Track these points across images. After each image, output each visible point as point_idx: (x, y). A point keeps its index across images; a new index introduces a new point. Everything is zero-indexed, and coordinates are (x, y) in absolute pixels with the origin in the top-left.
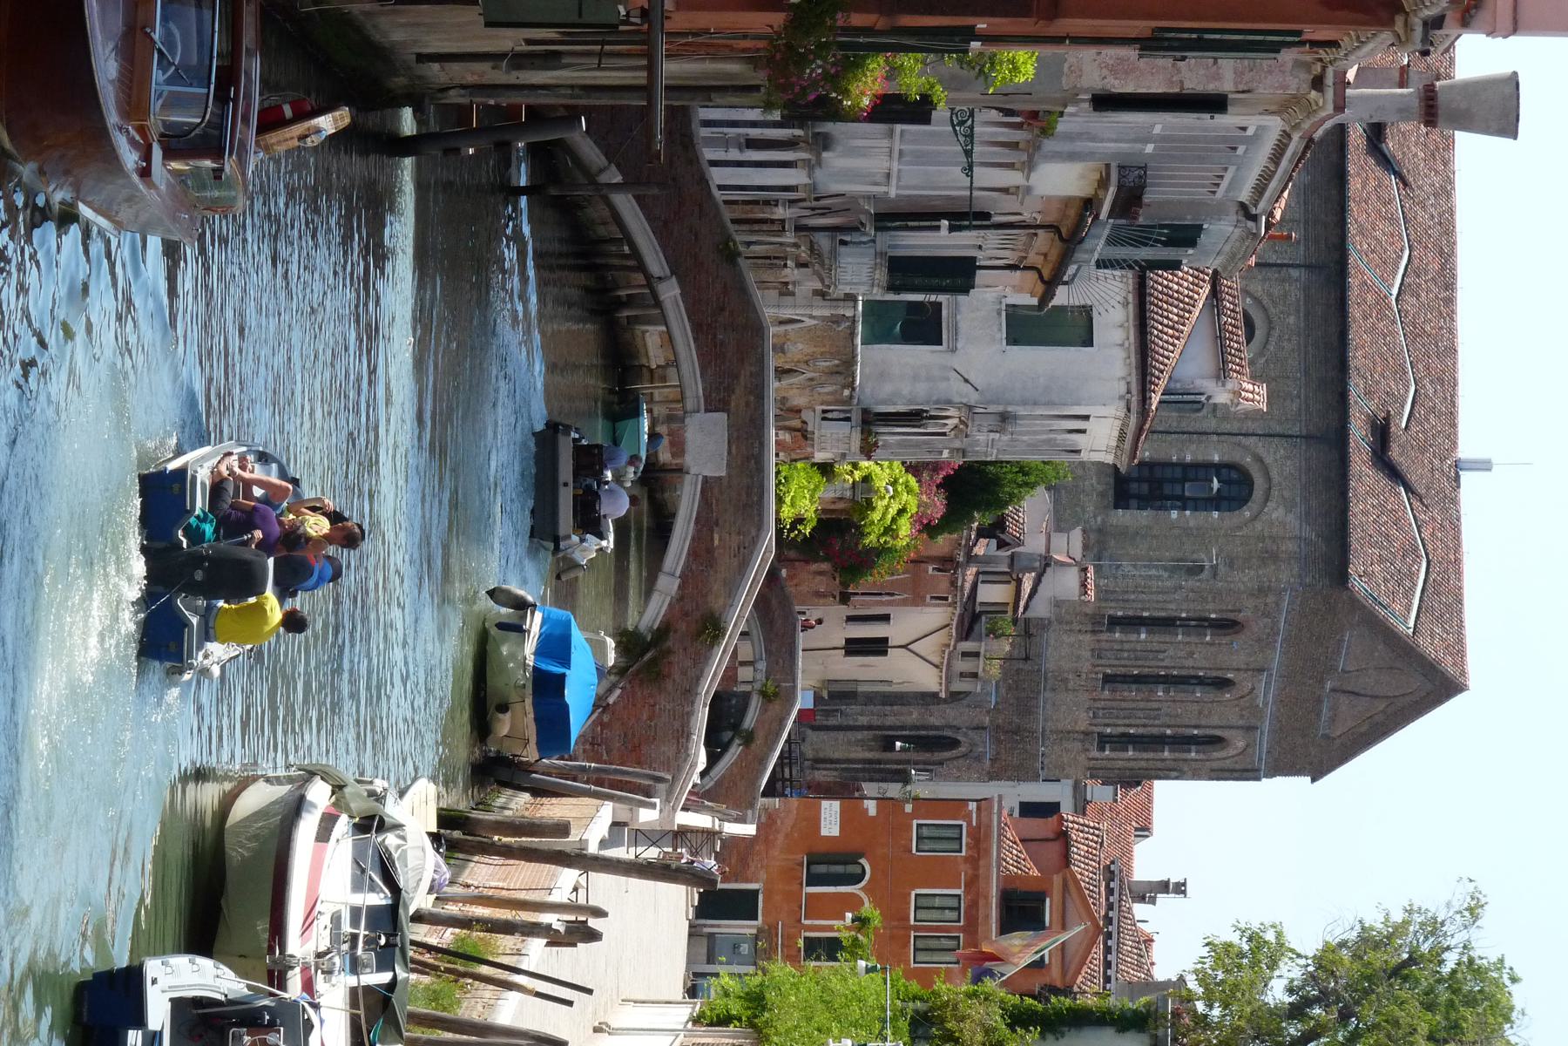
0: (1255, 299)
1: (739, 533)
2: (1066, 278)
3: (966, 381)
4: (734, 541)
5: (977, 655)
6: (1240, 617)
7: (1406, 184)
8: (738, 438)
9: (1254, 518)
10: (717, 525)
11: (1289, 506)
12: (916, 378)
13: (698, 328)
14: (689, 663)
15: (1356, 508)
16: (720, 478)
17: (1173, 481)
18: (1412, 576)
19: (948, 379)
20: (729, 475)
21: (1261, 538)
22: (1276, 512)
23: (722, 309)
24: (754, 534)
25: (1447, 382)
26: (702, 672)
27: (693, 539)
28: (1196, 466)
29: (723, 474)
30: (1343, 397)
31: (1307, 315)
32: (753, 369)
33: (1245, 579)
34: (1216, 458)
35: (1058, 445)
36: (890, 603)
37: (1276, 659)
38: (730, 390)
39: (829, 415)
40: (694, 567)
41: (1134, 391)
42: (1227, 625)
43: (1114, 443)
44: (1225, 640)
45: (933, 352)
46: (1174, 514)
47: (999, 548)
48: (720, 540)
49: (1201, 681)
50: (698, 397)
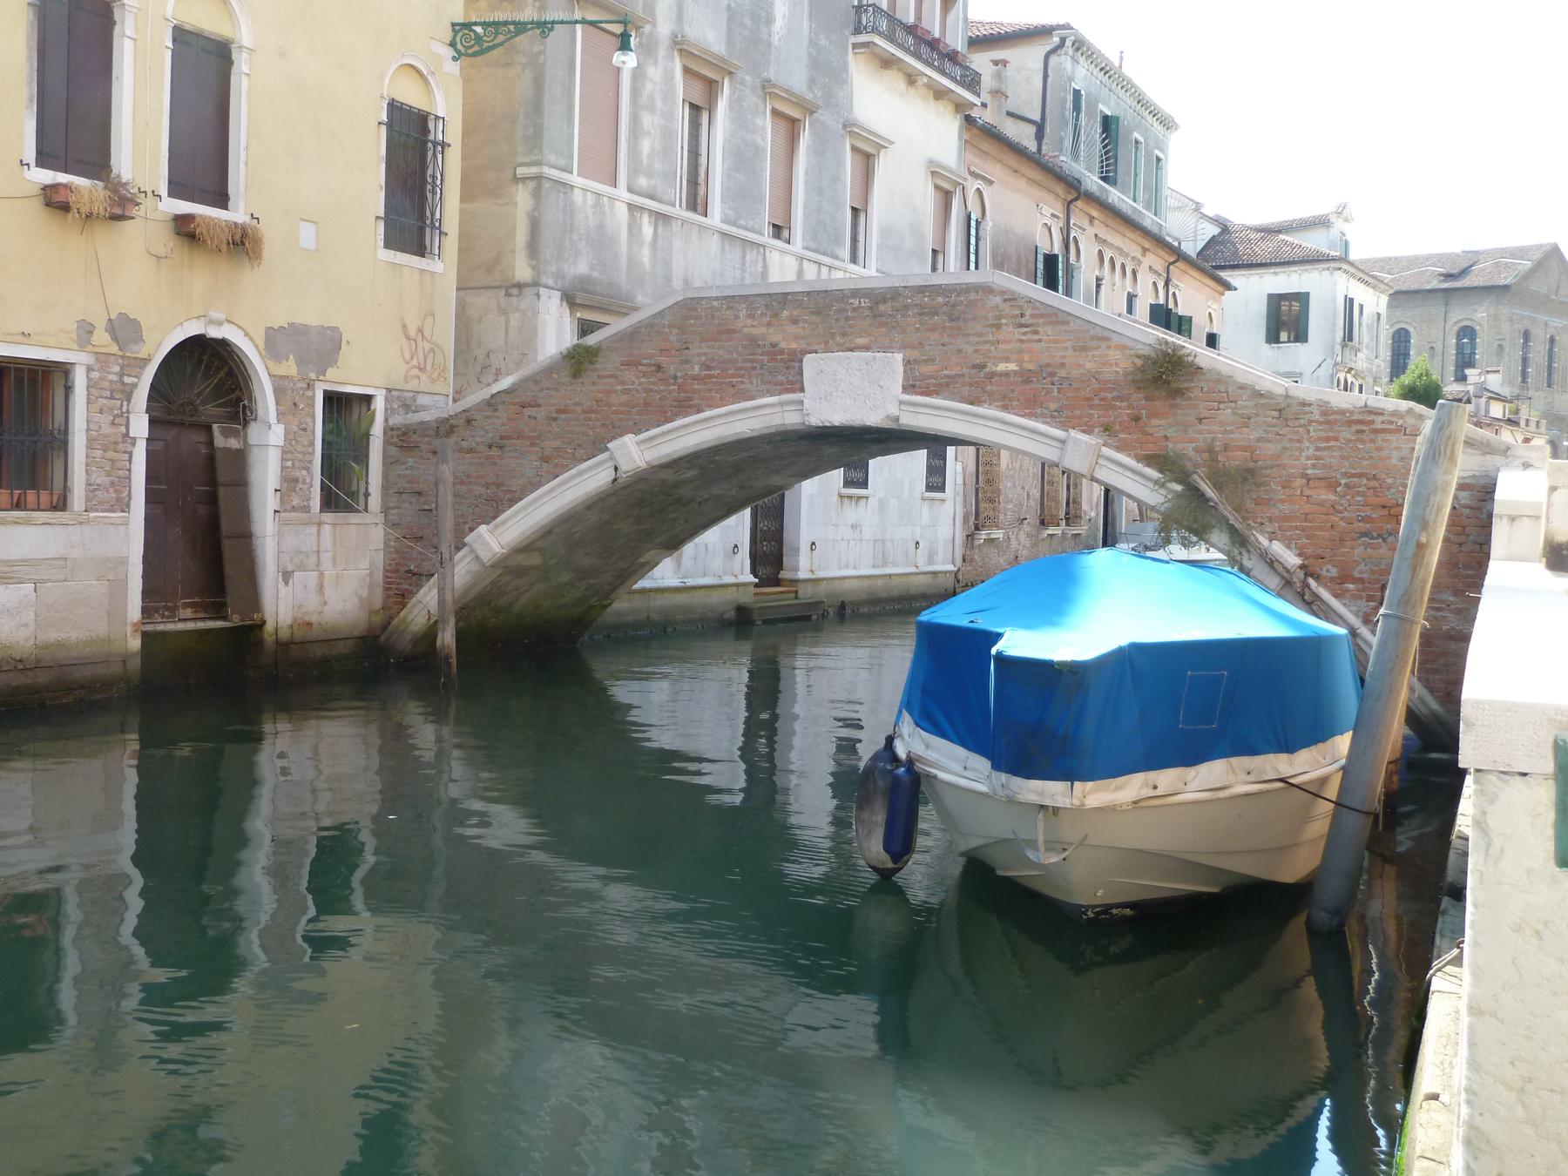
1: (998, 327)
2: (1176, 244)
4: (1010, 332)
5: (1527, 420)
6: (1522, 331)
8: (844, 334)
9: (1480, 324)
10: (982, 367)
13: (685, 406)
14: (1226, 413)
15: (1476, 284)
16: (907, 363)
17: (1463, 357)
18: (1506, 263)
20: (904, 347)
23: (659, 368)
25: (1428, 258)
26: (1243, 387)
27: (1005, 408)
29: (899, 357)
30: (1430, 291)
32: (743, 314)
33: (1506, 327)
35: (1373, 325)
37: (1542, 317)
38: (774, 351)
40: (1053, 406)
41: (1327, 265)
42: (1526, 335)
43: (1371, 290)
44: (1532, 337)
46: (1477, 357)
47: (1470, 403)
48: (1007, 360)
49: (1551, 349)
50: (781, 404)
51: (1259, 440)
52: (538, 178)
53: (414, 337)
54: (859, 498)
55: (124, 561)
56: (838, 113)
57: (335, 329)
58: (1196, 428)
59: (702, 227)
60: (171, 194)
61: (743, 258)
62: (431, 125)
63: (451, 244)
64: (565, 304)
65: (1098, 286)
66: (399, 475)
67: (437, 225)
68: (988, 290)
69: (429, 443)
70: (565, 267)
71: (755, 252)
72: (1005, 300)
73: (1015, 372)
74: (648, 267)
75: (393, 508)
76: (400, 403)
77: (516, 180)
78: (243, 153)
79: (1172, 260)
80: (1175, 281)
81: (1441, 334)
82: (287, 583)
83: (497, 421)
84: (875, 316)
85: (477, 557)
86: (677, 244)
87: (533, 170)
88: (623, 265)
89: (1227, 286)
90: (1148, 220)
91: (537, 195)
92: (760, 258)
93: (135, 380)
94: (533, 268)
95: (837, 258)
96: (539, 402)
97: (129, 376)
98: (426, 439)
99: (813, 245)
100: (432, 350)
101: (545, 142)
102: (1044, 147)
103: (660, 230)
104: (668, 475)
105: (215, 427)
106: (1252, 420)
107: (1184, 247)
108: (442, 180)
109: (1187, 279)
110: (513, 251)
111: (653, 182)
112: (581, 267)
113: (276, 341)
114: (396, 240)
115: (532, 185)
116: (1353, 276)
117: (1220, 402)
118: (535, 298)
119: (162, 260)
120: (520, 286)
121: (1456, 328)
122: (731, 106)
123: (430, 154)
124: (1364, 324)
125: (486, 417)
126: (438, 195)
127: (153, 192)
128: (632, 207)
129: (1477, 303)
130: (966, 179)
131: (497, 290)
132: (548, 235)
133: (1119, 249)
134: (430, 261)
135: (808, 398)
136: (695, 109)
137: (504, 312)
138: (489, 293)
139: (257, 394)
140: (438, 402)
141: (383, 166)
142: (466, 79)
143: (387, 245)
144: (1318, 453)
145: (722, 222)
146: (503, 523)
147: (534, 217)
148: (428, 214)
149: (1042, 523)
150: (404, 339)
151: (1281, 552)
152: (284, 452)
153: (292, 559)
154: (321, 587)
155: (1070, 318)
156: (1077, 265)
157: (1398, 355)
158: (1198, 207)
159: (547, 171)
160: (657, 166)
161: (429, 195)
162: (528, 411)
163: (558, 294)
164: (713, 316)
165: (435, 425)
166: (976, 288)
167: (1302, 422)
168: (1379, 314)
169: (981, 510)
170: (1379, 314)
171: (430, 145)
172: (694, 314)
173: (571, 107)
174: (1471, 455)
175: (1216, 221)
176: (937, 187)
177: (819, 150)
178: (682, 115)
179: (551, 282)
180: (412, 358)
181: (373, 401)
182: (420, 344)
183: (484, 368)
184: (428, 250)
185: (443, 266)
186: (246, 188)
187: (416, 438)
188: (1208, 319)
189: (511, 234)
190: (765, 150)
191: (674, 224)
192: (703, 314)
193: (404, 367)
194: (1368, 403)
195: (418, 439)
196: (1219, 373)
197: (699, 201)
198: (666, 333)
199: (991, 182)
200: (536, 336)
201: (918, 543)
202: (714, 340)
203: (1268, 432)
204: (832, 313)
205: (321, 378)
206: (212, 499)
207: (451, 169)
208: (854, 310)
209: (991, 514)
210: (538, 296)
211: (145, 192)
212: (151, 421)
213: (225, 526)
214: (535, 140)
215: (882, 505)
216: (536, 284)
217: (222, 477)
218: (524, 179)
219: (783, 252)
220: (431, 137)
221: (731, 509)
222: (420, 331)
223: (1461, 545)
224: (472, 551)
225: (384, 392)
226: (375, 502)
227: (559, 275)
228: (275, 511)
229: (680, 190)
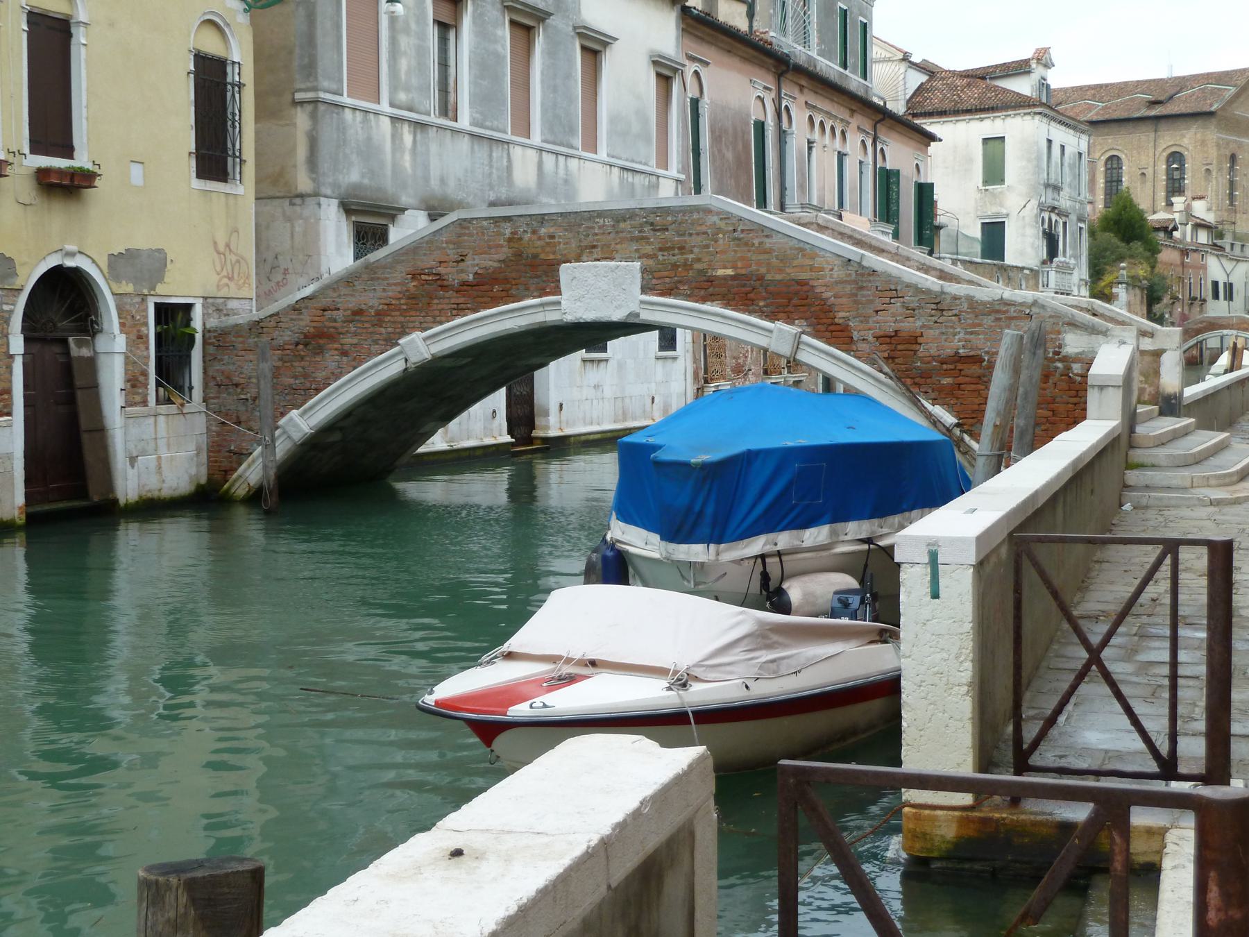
0: (1102, 155)
2: (882, 103)
3: (1025, 207)
7: (1060, 103)
11: (1183, 136)
12: (1023, 235)
14: (897, 305)
16: (644, 271)
19: (1024, 217)
21: (1195, 147)
22: (1186, 141)
24: (715, 219)
25: (1138, 83)
26: (908, 286)
28: (1167, 174)
29: (637, 265)
31: (1107, 135)
34: (1164, 167)
35: (1075, 164)
36: (1206, 281)
39: (1046, 283)
43: (1072, 132)
44: (1239, 162)
45: (1009, 226)
48: (725, 268)
50: (542, 305)
51: (923, 326)
52: (315, 102)
53: (223, 252)
54: (600, 361)
55: (9, 456)
56: (568, 17)
57: (160, 251)
58: (875, 319)
59: (455, 131)
60: (33, 151)
61: (490, 156)
62: (229, 69)
63: (250, 170)
64: (341, 210)
65: (810, 148)
66: (218, 370)
67: (237, 154)
68: (707, 211)
69: (242, 342)
70: (341, 177)
71: (500, 148)
72: (721, 219)
73: (733, 278)
74: (409, 170)
75: (213, 398)
76: (214, 309)
77: (295, 103)
78: (84, 111)
79: (878, 119)
80: (882, 136)
81: (1151, 160)
82: (133, 467)
83: (302, 323)
84: (617, 232)
85: (289, 437)
86: (434, 148)
87: (310, 95)
88: (389, 172)
89: (931, 138)
90: (853, 81)
91: (314, 116)
92: (505, 155)
93: (12, 307)
94: (314, 180)
95: (572, 147)
96: (339, 305)
97: (7, 304)
98: (241, 339)
99: (550, 138)
100: (238, 261)
101: (319, 71)
102: (755, 24)
103: (419, 136)
104: (448, 363)
105: (71, 339)
106: (917, 312)
107: (889, 106)
108: (240, 116)
109: (894, 135)
110: (295, 166)
111: (410, 96)
112: (354, 176)
113: (121, 263)
114: (202, 173)
115: (309, 108)
116: (1053, 119)
117: (891, 298)
118: (316, 207)
119: (28, 207)
120: (302, 196)
121: (1165, 154)
122: (474, 22)
123: (229, 95)
124: (1066, 164)
125: (292, 319)
126: (237, 129)
127: (19, 151)
128: (394, 119)
129: (1185, 129)
130: (684, 66)
131: (281, 200)
132: (325, 150)
133: (828, 113)
134: (233, 186)
135: (566, 298)
136: (443, 27)
137: (289, 219)
138: (276, 202)
139: (102, 309)
140: (246, 310)
141: (193, 109)
142: (253, 23)
143: (199, 176)
144: (967, 336)
145: (470, 125)
146: (311, 408)
147: (313, 136)
148: (229, 145)
149: (766, 372)
150: (215, 254)
151: (941, 414)
152: (127, 358)
153: (136, 446)
154: (159, 467)
155: (773, 233)
156: (789, 131)
157: (1112, 182)
158: (906, 58)
159: (322, 95)
160: (414, 81)
161: (230, 129)
162: (328, 314)
163: (335, 203)
164: (483, 234)
165: (247, 327)
166: (697, 209)
167: (954, 312)
168: (1080, 154)
169: (709, 365)
170: (1080, 154)
171: (229, 87)
172: (467, 232)
173: (339, 37)
174: (1081, 335)
175: (923, 67)
176: (659, 75)
177: (551, 53)
178: (432, 33)
179: (329, 192)
180: (222, 269)
181: (193, 309)
182: (229, 257)
183: (273, 268)
184: (231, 176)
185: (243, 188)
186: (89, 139)
187: (231, 338)
188: (915, 170)
189: (293, 150)
190: (505, 57)
191: (430, 131)
192: (475, 232)
193: (215, 278)
194: (1004, 297)
195: (234, 339)
196: (890, 275)
197: (450, 107)
198: (444, 248)
199: (707, 64)
200: (319, 240)
201: (653, 398)
202: (485, 253)
203: (929, 321)
204: (581, 230)
205: (152, 293)
206: (71, 400)
207: (246, 106)
208: (600, 227)
209: (718, 367)
210: (319, 205)
211: (14, 153)
212: (26, 340)
213: (84, 423)
214: (310, 68)
215: (621, 366)
216: (316, 194)
217: (78, 382)
218: (302, 103)
219: (525, 146)
220: (229, 79)
221: (494, 388)
222: (228, 245)
223: (1075, 404)
224: (285, 432)
225: (201, 300)
226: (197, 393)
227: (335, 185)
228: (122, 407)
229: (433, 102)
